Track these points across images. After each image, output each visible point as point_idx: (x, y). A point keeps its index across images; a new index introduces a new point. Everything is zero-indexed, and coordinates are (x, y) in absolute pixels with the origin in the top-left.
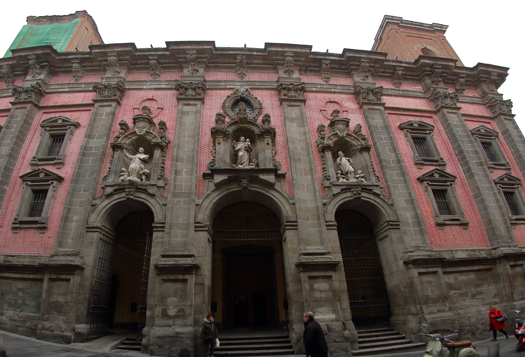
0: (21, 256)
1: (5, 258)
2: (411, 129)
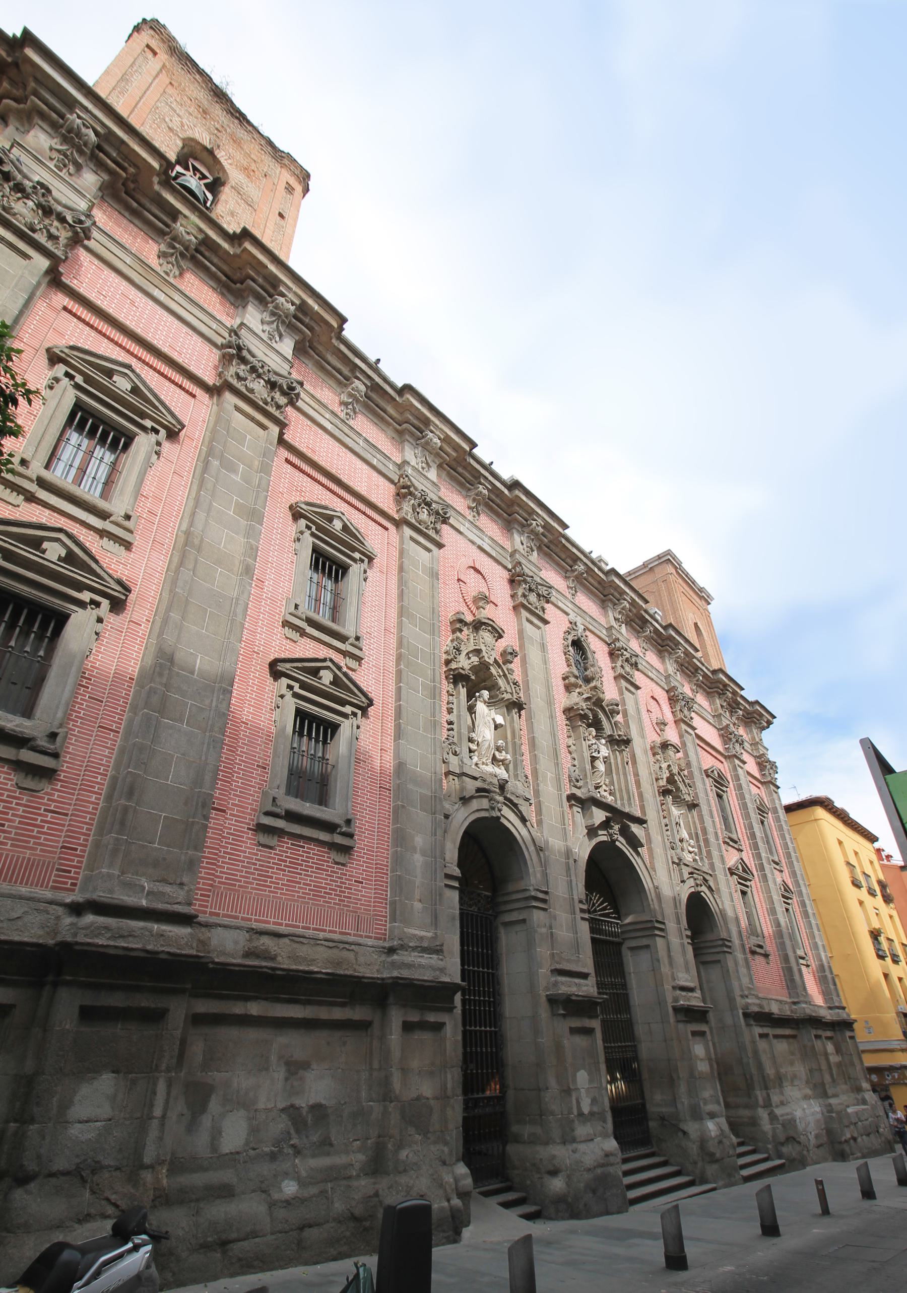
0: (304, 937)
1: (250, 940)
2: (319, 528)
